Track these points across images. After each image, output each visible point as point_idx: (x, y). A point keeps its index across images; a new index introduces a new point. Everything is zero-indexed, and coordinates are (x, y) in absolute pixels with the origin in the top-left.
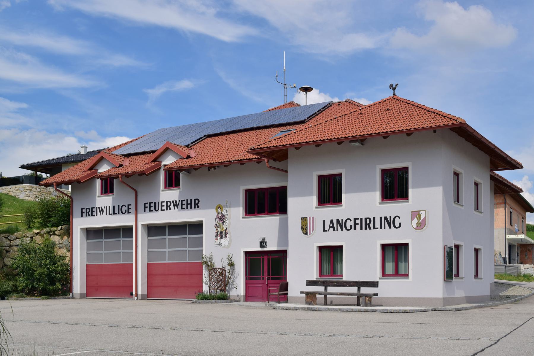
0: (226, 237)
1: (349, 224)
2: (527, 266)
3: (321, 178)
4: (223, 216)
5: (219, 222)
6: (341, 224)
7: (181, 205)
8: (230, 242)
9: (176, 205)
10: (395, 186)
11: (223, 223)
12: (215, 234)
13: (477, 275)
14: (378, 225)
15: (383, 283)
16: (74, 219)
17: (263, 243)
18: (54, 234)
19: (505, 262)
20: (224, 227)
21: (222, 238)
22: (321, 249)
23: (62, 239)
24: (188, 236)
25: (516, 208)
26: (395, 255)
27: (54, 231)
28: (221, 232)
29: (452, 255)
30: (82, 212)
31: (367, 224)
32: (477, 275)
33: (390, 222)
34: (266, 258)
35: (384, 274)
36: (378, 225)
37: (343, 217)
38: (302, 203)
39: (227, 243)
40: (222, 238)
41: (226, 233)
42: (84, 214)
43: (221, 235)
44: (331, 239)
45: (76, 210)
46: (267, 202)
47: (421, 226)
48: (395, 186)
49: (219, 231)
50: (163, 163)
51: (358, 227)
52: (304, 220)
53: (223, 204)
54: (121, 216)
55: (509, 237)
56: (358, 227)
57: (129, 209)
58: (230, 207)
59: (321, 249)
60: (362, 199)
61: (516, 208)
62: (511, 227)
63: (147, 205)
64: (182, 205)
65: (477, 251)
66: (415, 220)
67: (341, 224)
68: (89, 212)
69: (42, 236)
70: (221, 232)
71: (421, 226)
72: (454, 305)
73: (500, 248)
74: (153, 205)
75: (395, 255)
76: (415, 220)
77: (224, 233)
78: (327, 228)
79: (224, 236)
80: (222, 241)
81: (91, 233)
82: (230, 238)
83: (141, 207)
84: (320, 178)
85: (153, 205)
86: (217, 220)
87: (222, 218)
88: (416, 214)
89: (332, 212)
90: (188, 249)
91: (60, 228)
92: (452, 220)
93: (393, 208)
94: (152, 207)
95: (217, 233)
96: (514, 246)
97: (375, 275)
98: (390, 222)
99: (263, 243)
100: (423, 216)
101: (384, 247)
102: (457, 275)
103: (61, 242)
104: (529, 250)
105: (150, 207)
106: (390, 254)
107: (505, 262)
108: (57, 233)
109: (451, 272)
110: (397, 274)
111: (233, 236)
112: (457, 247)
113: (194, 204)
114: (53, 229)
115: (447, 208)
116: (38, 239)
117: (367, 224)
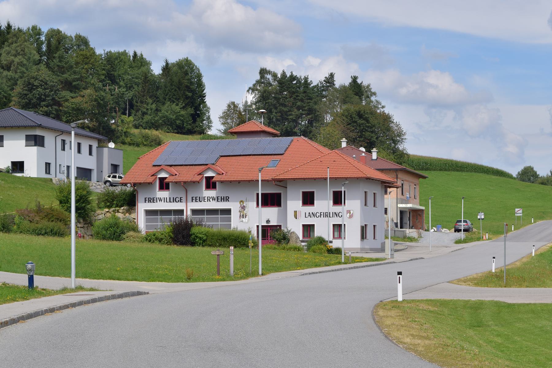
1: (318, 215)
2: (411, 230)
3: (304, 193)
4: (244, 206)
6: (314, 215)
7: (218, 199)
8: (248, 220)
9: (213, 199)
10: (338, 199)
13: (374, 238)
14: (331, 216)
15: (334, 241)
16: (139, 204)
17: (268, 221)
18: (118, 212)
19: (397, 226)
20: (245, 212)
22: (304, 226)
23: (125, 215)
24: (219, 216)
25: (407, 179)
26: (338, 228)
27: (118, 210)
29: (364, 229)
30: (145, 200)
31: (327, 215)
32: (374, 238)
33: (337, 215)
34: (269, 229)
35: (334, 238)
36: (331, 216)
37: (315, 212)
38: (293, 203)
39: (246, 221)
41: (246, 216)
42: (147, 201)
43: (243, 216)
44: (309, 221)
45: (140, 198)
46: (271, 200)
47: (351, 217)
48: (338, 199)
49: (242, 214)
50: (205, 175)
51: (322, 216)
52: (295, 212)
53: (244, 200)
54: (175, 203)
55: (400, 206)
56: (322, 216)
57: (181, 200)
59: (304, 226)
60: (323, 203)
61: (407, 179)
62: (402, 197)
63: (194, 198)
64: (218, 199)
65: (374, 226)
66: (348, 214)
67: (314, 215)
68: (151, 200)
69: (110, 213)
71: (351, 217)
73: (393, 215)
74: (198, 198)
75: (338, 228)
76: (348, 214)
78: (307, 216)
80: (244, 219)
81: (149, 213)
82: (248, 218)
83: (190, 199)
84: (303, 192)
85: (198, 198)
87: (243, 208)
88: (349, 212)
89: (309, 209)
90: (219, 223)
91: (122, 208)
92: (364, 214)
93: (338, 209)
94: (195, 199)
96: (406, 211)
97: (331, 238)
98: (337, 215)
99: (268, 221)
100: (352, 213)
101: (334, 225)
102: (366, 238)
103: (124, 217)
104: (419, 215)
105: (196, 199)
106: (336, 229)
107: (397, 226)
108: (120, 211)
109: (363, 236)
110: (340, 237)
111: (248, 217)
112: (366, 225)
113: (227, 199)
114: (117, 208)
115: (362, 211)
116: (108, 215)
117: (327, 215)
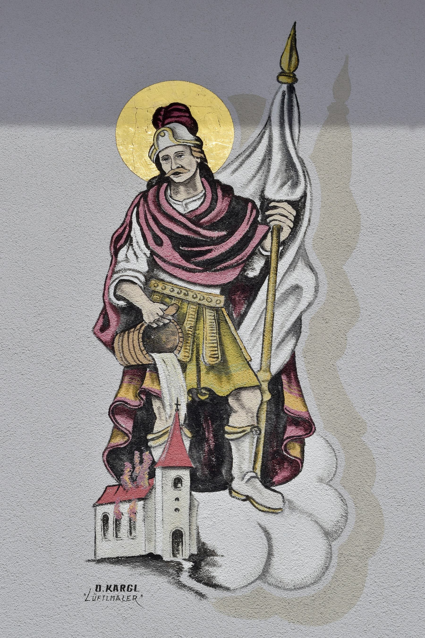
0: (278, 464)
4: (237, 212)
5: (173, 283)
8: (349, 544)
11: (242, 292)
12: (101, 433)
20: (257, 340)
21: (212, 475)
28: (207, 414)
39: (301, 555)
40: (212, 475)
49: (173, 386)
58: (338, 116)
70: (207, 414)
72: (209, 246)
77: (246, 413)
79: (244, 456)
80: (220, 518)
82: (354, 480)
86: (135, 261)
91: (122, 458)
95: (136, 419)
